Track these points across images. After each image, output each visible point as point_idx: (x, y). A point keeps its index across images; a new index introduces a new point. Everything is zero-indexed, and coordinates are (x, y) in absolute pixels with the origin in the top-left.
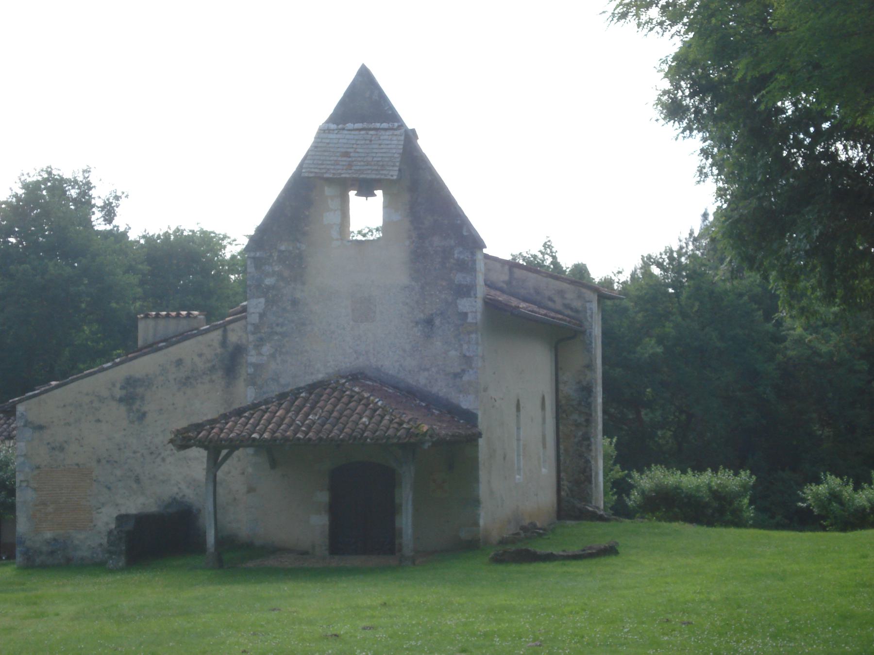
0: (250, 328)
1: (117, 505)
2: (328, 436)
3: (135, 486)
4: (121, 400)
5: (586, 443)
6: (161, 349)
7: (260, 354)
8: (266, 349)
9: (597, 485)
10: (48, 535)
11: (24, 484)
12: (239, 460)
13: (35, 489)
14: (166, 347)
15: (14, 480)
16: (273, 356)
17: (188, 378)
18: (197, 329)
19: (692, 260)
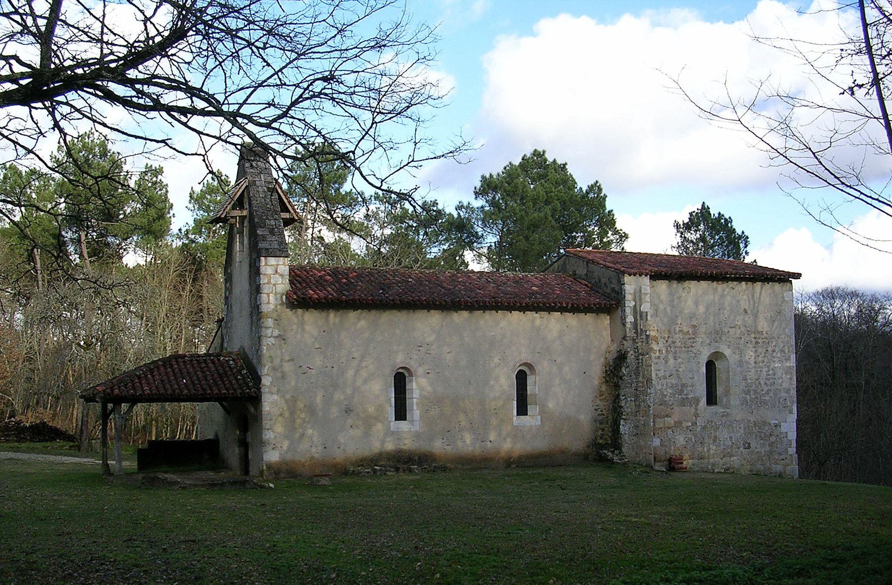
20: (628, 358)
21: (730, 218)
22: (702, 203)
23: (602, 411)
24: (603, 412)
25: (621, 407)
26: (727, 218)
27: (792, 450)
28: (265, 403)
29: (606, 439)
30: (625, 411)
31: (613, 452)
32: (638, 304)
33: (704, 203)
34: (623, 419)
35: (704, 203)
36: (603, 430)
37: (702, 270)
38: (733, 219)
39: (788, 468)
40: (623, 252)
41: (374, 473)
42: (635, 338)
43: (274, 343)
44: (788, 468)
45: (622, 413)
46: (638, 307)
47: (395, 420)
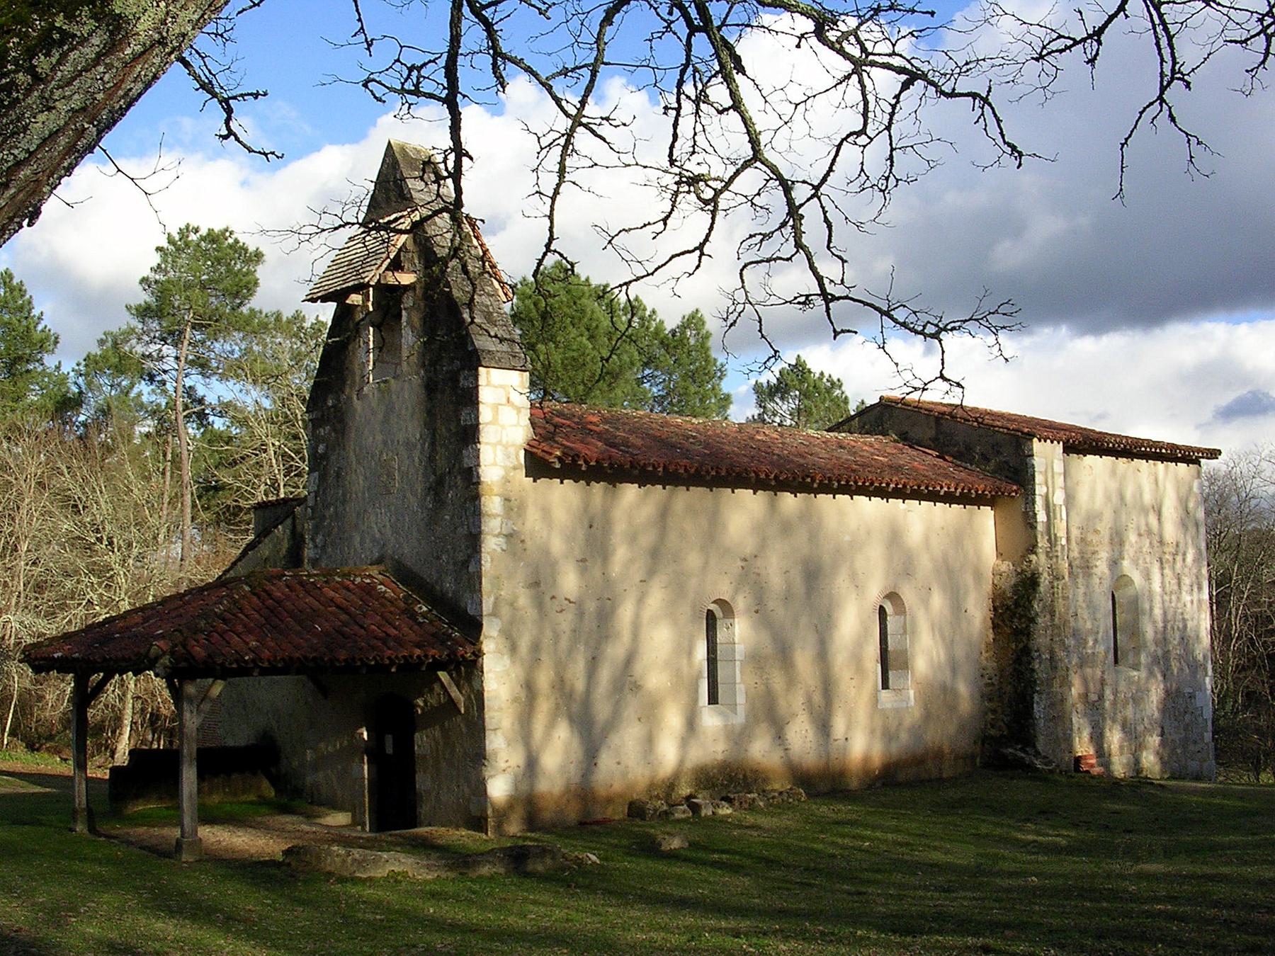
5: (1025, 659)
20: (1042, 585)
21: (839, 380)
22: (796, 356)
23: (990, 679)
24: (993, 680)
25: (1033, 670)
26: (835, 380)
27: (1208, 736)
28: (490, 675)
29: (1000, 729)
30: (1039, 678)
31: (1023, 750)
32: (1051, 489)
33: (799, 356)
34: (1037, 691)
35: (799, 356)
36: (994, 711)
37: (654, 458)
38: (843, 382)
39: (1205, 765)
40: (867, 407)
41: (694, 813)
42: (1048, 550)
43: (504, 548)
44: (1205, 765)
45: (1035, 682)
46: (1050, 496)
47: (709, 704)
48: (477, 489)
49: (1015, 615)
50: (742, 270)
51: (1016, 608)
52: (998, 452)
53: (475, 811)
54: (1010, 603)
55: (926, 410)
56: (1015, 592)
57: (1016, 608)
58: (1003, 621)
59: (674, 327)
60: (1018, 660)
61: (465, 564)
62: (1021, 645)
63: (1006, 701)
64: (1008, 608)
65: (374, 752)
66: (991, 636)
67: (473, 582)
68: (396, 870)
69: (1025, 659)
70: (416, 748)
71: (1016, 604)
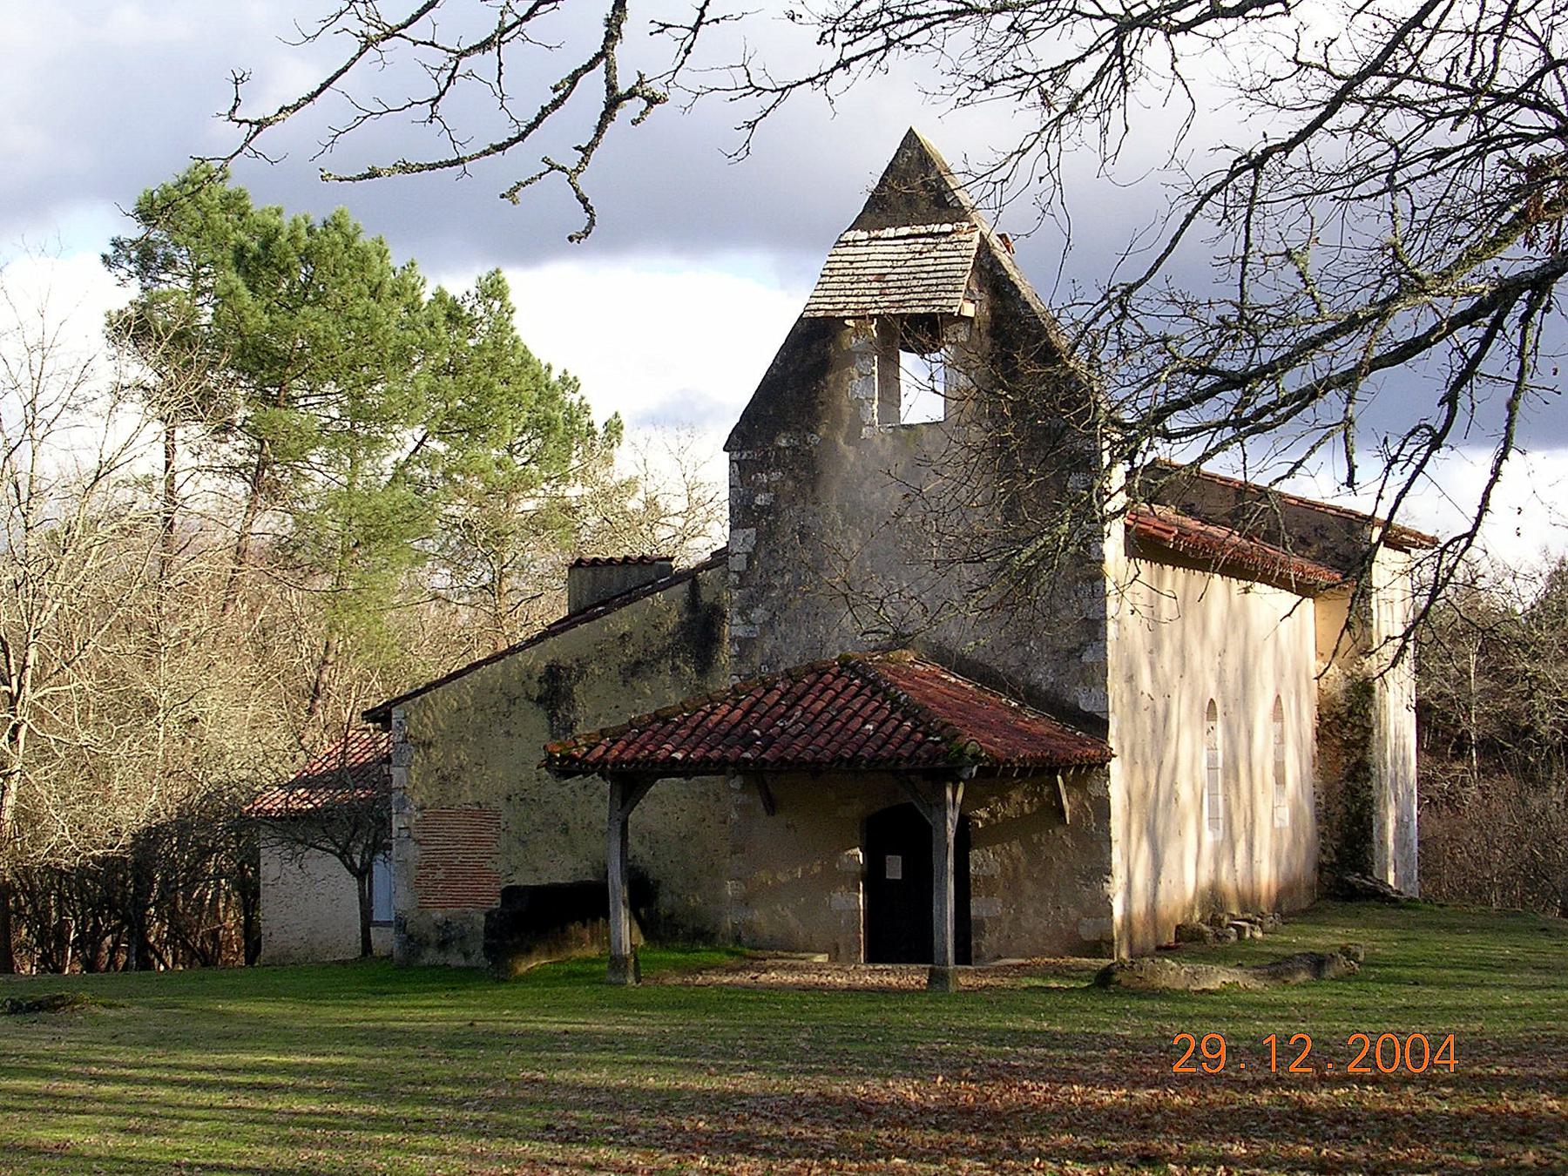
0: (734, 577)
1: (536, 870)
2: (855, 753)
3: (562, 839)
4: (540, 700)
5: (1361, 775)
6: (598, 615)
7: (749, 622)
8: (758, 614)
9: (1383, 843)
10: (438, 915)
11: (405, 833)
12: (718, 800)
13: (418, 842)
14: (606, 613)
15: (1324, 858)
16: (769, 625)
17: (638, 663)
18: (652, 582)
19: (392, 315)
21: (575, 379)
48: (1100, 568)
49: (1345, 725)
50: (592, 222)
51: (1349, 716)
52: (1323, 536)
53: (1088, 933)
54: (1342, 711)
55: (1221, 479)
56: (1348, 699)
57: (1349, 716)
58: (1331, 732)
59: (511, 298)
60: (1352, 777)
61: (1075, 653)
62: (1353, 760)
63: (1335, 824)
64: (1338, 716)
65: (873, 876)
66: (1316, 748)
67: (1096, 675)
68: (1227, 981)
69: (1361, 775)
70: (972, 868)
71: (1350, 712)
